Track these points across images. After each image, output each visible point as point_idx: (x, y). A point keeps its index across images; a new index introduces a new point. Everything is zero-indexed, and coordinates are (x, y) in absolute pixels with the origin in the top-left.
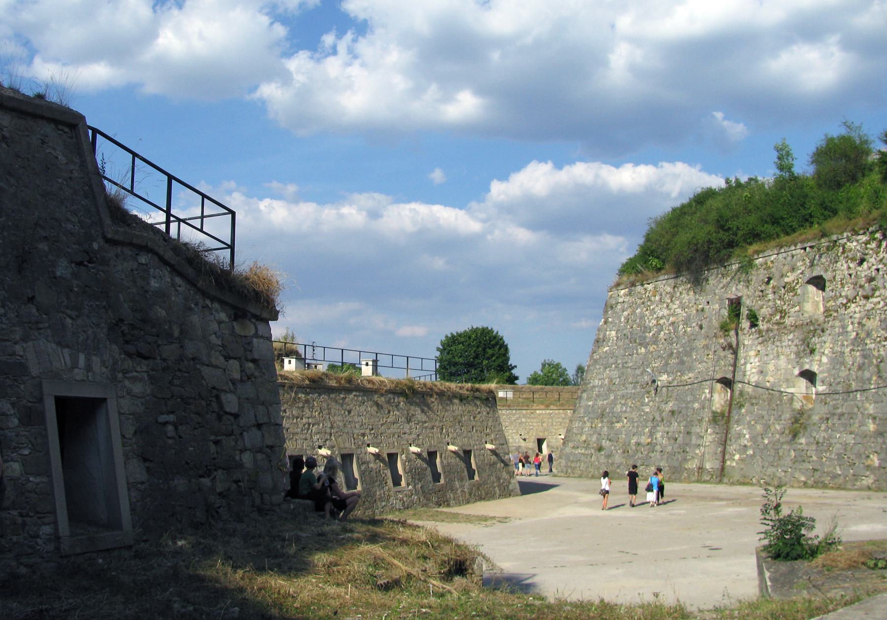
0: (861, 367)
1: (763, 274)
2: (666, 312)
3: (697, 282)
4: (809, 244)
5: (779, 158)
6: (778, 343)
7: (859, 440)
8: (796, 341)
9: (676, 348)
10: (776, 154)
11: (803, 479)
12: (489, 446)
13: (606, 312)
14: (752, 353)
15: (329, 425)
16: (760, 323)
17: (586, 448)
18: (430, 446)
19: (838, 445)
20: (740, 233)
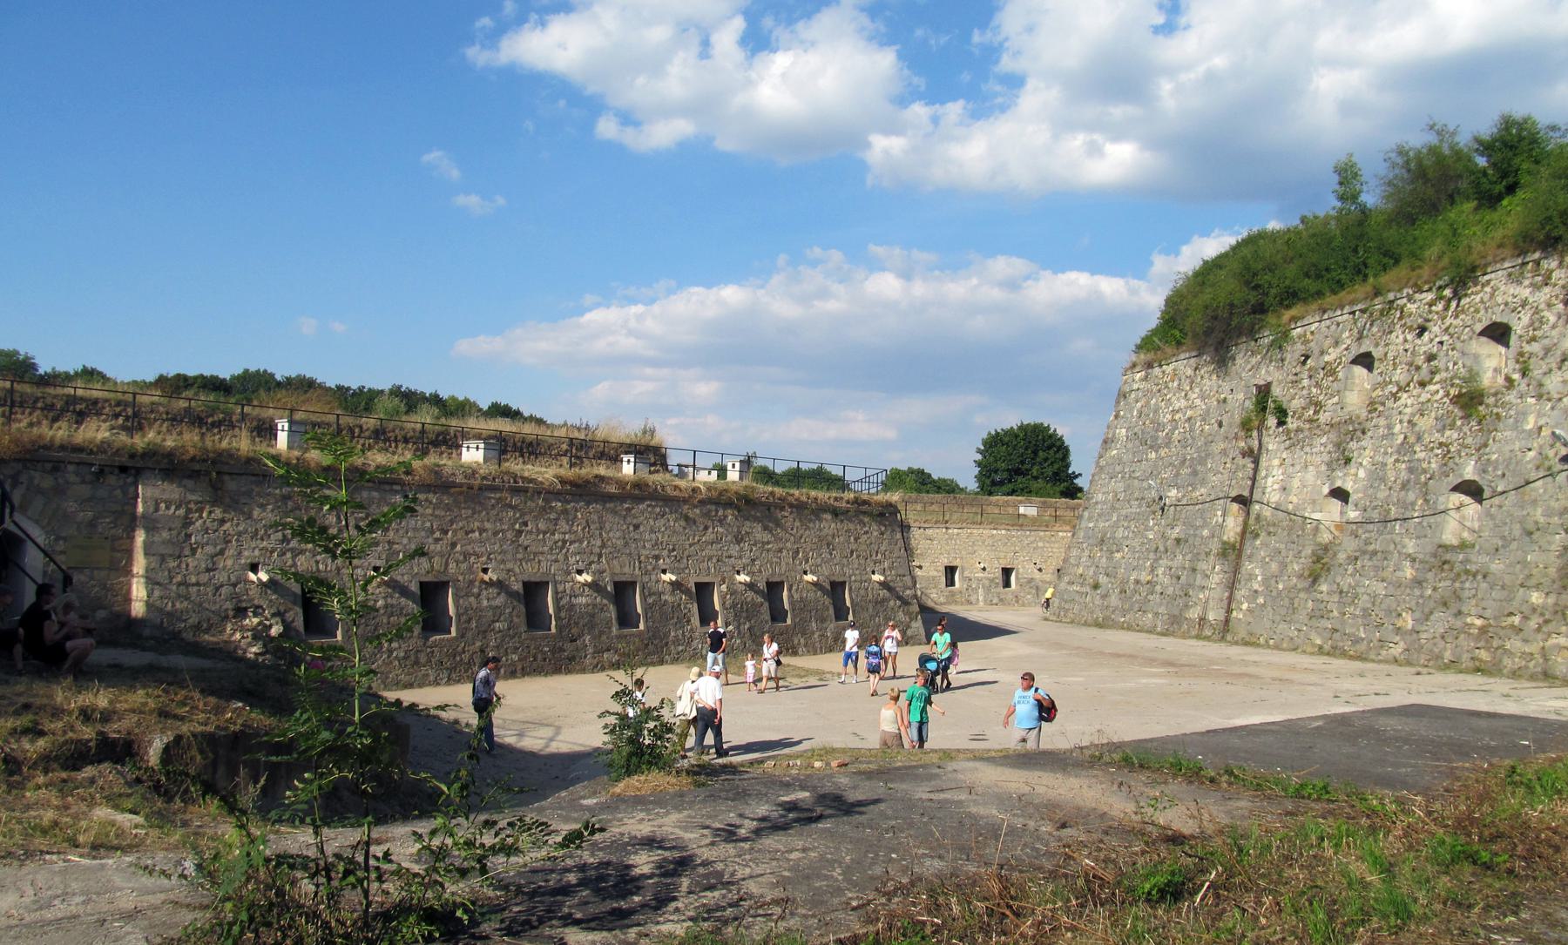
0: (1404, 486)
1: (1299, 348)
2: (1183, 403)
3: (1222, 361)
4: (1360, 306)
5: (1341, 184)
6: (1307, 449)
7: (1391, 590)
8: (1330, 447)
9: (1191, 453)
10: (1336, 178)
11: (1319, 642)
12: (877, 577)
13: (1118, 402)
14: (1276, 462)
15: (599, 543)
16: (1289, 420)
17: (1082, 585)
18: (773, 574)
19: (1366, 597)
20: (1273, 291)
